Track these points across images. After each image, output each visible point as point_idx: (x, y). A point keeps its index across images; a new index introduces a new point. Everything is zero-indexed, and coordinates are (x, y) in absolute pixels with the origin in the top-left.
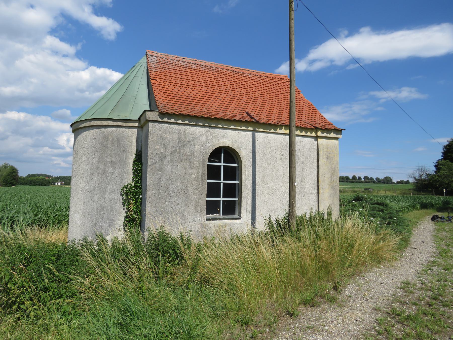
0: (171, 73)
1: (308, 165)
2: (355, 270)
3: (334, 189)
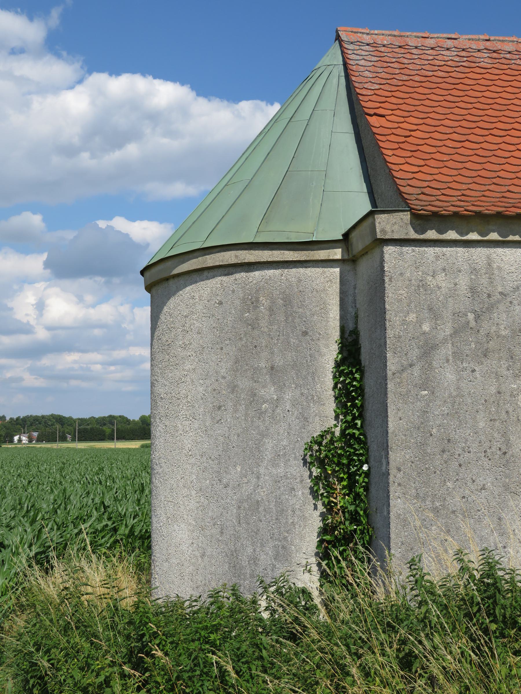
0: (421, 90)
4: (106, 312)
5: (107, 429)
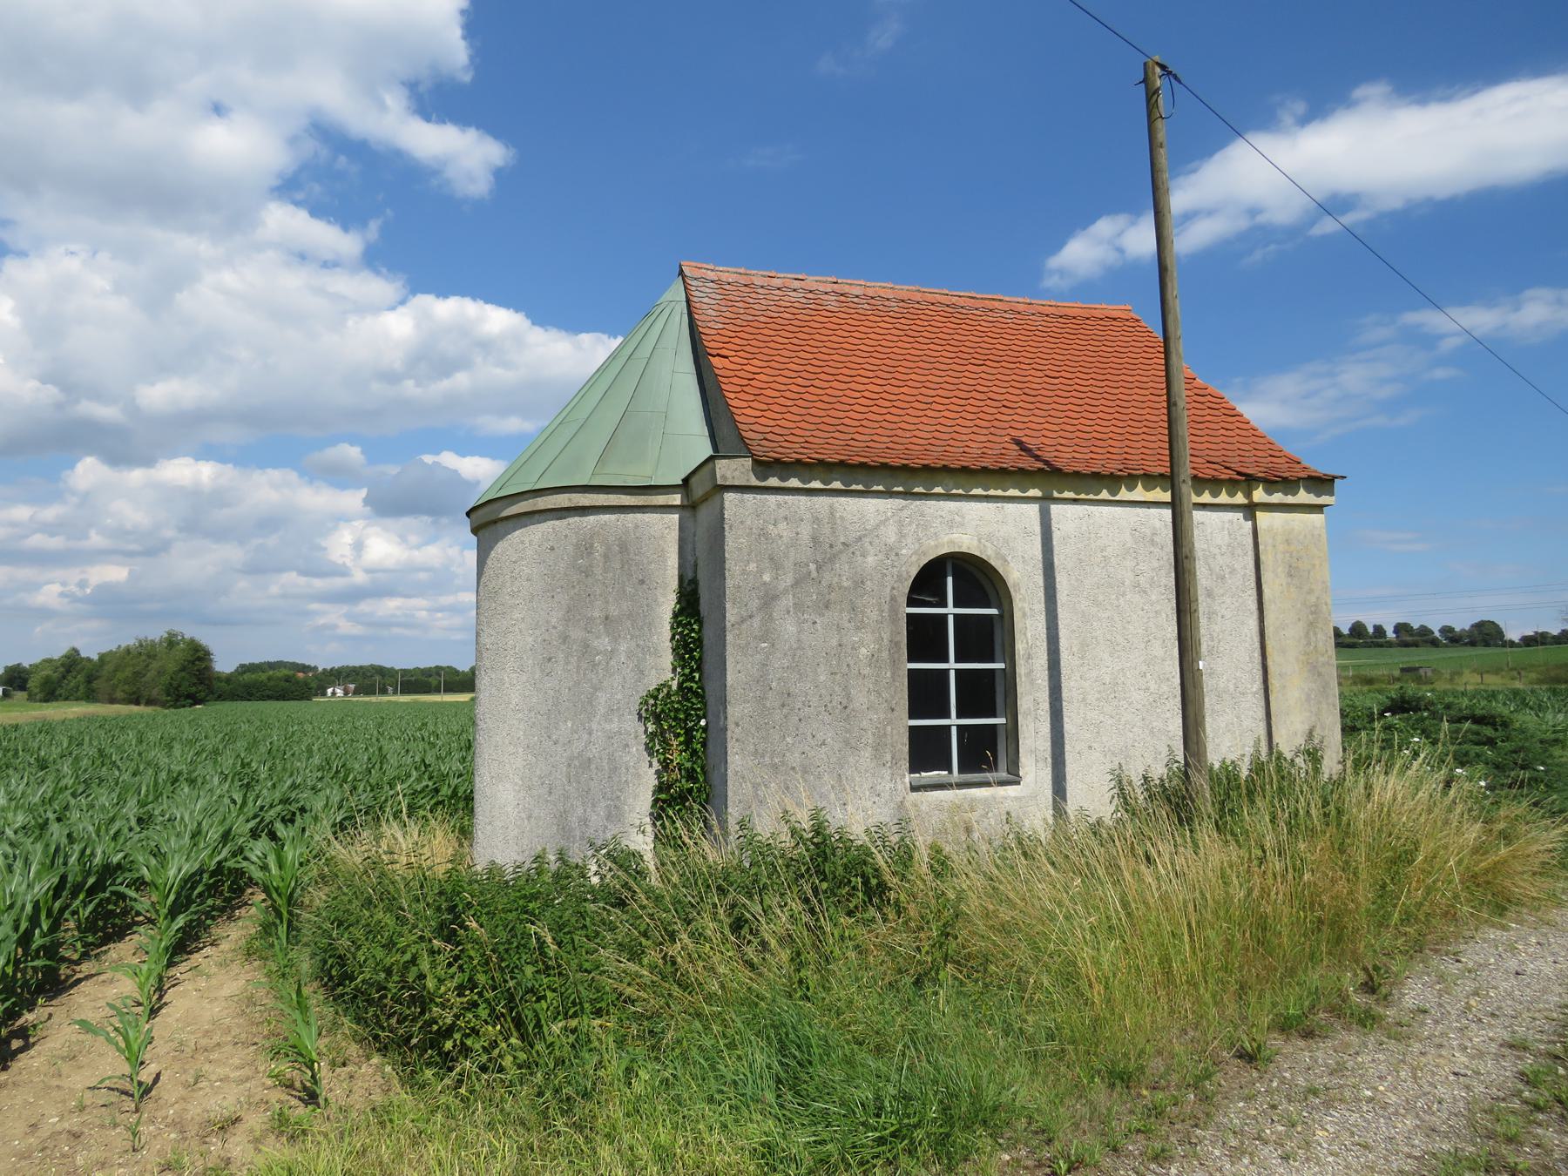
0: (766, 331)
1: (1228, 601)
2: (1425, 934)
3: (1320, 674)
4: (432, 554)
5: (433, 681)
